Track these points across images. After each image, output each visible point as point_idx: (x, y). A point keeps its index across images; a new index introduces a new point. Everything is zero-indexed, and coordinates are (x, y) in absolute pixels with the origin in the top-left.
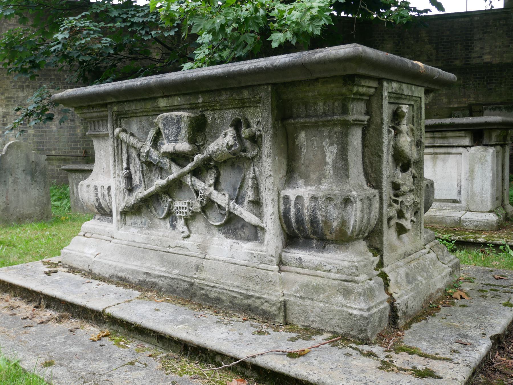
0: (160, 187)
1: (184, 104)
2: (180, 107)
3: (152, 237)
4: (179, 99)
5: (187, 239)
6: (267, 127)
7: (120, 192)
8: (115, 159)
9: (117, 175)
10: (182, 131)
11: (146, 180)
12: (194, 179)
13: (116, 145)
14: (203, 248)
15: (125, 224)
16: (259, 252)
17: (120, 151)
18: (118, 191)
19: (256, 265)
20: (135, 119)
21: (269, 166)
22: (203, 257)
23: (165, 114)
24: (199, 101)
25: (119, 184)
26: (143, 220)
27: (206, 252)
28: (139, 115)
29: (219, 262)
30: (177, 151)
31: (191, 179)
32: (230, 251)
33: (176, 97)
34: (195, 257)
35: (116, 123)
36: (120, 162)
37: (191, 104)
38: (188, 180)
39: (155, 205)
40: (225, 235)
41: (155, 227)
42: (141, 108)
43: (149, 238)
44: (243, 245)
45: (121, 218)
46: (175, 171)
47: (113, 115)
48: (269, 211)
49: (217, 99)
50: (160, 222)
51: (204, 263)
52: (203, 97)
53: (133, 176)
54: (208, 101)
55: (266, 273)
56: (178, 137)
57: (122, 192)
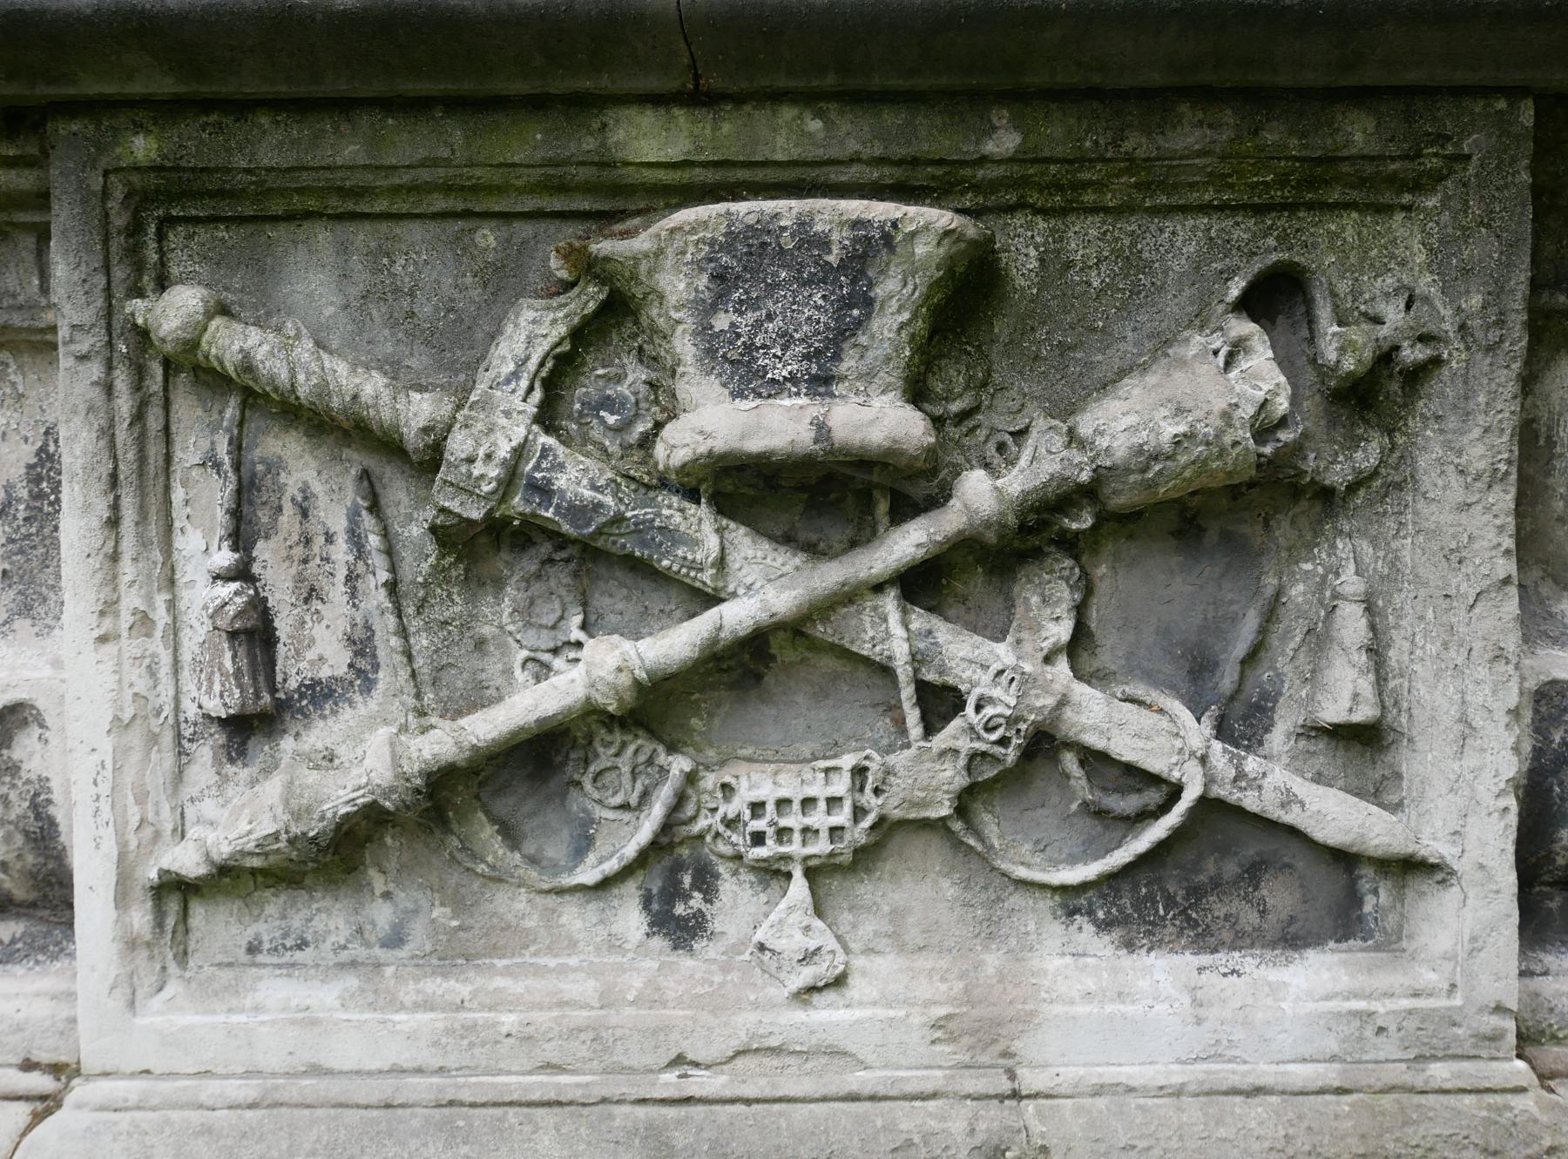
0: (637, 683)
1: (854, 160)
2: (813, 173)
3: (509, 1020)
4: (815, 125)
5: (830, 996)
6: (1500, 323)
7: (153, 739)
8: (115, 507)
9: (126, 619)
10: (875, 324)
11: (421, 642)
12: (920, 620)
13: (124, 405)
14: (984, 1036)
15: (183, 957)
16: (1406, 1003)
17: (154, 450)
18: (135, 738)
19: (1398, 1073)
20: (323, 236)
21: (1501, 528)
22: (1005, 1086)
23: (741, 208)
24: (990, 147)
25: (142, 686)
26: (382, 915)
27: (1006, 1054)
28: (381, 206)
29: (1133, 1101)
30: (845, 450)
31: (905, 624)
32: (1199, 1021)
33: (788, 113)
34: (934, 1096)
35: (134, 254)
36: (153, 531)
37: (914, 162)
38: (891, 631)
39: (502, 806)
40: (1117, 933)
41: (495, 950)
42: (431, 163)
43: (472, 1027)
44: (1274, 974)
45: (159, 923)
46: (763, 584)
47: (105, 194)
48: (1487, 775)
49: (1136, 143)
50: (550, 914)
51: (1037, 1127)
52: (1017, 124)
53: (283, 626)
54: (1060, 151)
55: (1499, 1110)
56: (837, 357)
57: (167, 738)
